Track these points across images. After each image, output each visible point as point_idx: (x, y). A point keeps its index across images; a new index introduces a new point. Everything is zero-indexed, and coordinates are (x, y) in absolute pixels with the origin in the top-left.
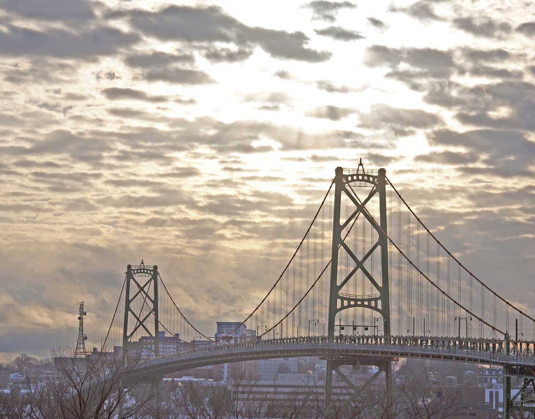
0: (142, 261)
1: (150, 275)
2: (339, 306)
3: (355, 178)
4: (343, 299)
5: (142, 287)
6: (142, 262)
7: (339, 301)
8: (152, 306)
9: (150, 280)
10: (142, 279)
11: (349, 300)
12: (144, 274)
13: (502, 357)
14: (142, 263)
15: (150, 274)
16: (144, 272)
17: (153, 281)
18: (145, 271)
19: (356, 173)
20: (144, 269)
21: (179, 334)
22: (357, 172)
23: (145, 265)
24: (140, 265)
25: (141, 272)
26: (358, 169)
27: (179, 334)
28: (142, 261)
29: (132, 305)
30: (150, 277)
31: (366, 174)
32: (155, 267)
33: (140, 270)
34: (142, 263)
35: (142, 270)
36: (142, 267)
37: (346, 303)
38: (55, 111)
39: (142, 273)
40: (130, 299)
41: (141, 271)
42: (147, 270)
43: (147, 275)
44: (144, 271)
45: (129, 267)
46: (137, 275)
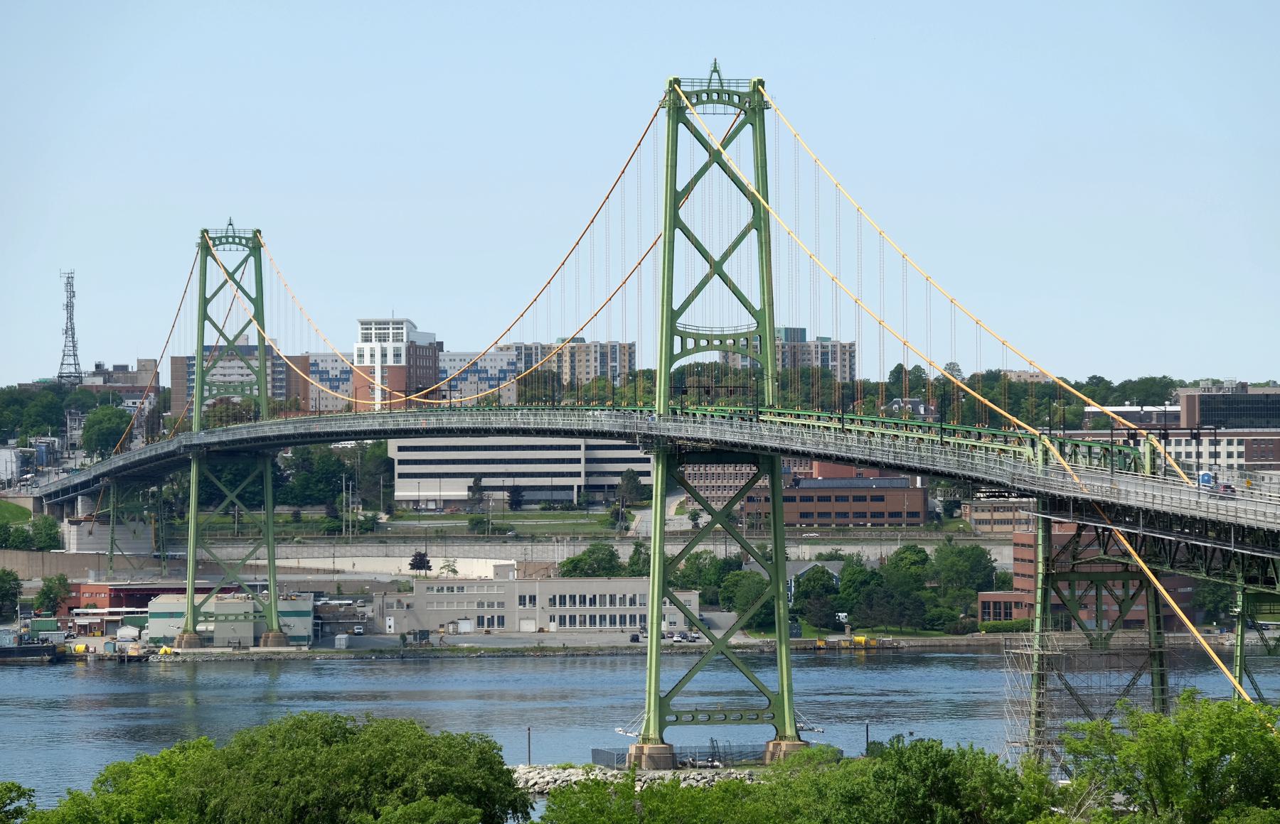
0: (715, 63)
1: (246, 249)
2: (677, 350)
3: (704, 97)
5: (231, 271)
6: (715, 67)
7: (677, 340)
8: (251, 309)
9: (245, 260)
10: (231, 256)
11: (697, 337)
12: (234, 247)
13: (943, 456)
14: (715, 70)
15: (246, 246)
16: (234, 243)
17: (252, 259)
18: (237, 240)
19: (706, 88)
20: (234, 237)
21: (594, 751)
22: (709, 86)
23: (235, 228)
24: (225, 227)
25: (228, 242)
26: (710, 80)
27: (594, 751)
28: (715, 63)
29: (211, 310)
30: (247, 251)
31: (726, 88)
33: (227, 237)
34: (715, 70)
35: (229, 239)
37: (690, 343)
38: (387, 579)
39: (231, 243)
40: (208, 296)
41: (227, 240)
42: (240, 238)
43: (240, 248)
44: (227, 240)
46: (221, 247)
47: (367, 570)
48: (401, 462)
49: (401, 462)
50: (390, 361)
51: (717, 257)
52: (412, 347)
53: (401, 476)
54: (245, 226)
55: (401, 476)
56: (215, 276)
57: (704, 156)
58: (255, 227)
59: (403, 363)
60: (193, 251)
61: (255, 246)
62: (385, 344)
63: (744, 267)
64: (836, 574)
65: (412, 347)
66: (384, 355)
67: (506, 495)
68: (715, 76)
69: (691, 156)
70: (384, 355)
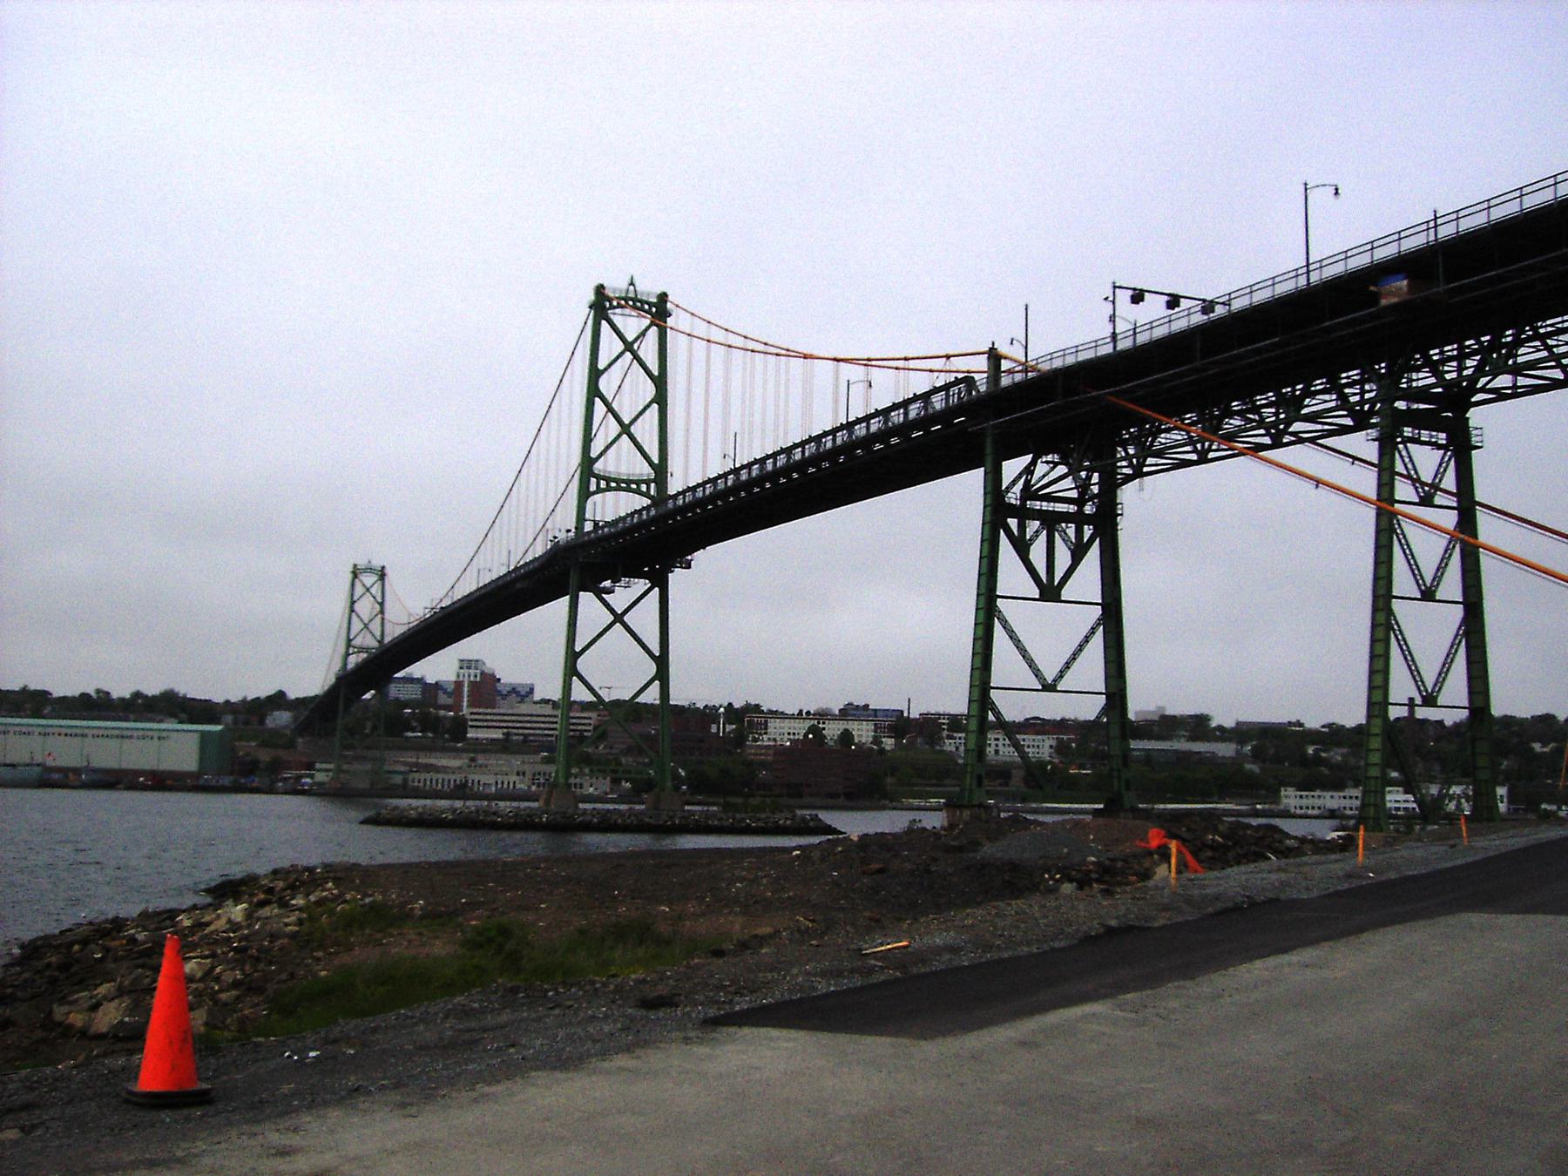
2: (593, 488)
4: (599, 478)
7: (593, 480)
10: (368, 580)
11: (608, 480)
14: (632, 284)
30: (376, 578)
32: (383, 568)
34: (632, 284)
35: (369, 570)
36: (631, 295)
45: (600, 290)
47: (970, 664)
48: (472, 720)
49: (472, 720)
50: (472, 679)
51: (627, 422)
52: (482, 673)
53: (471, 727)
54: (377, 563)
55: (471, 727)
56: (359, 590)
57: (620, 346)
58: (382, 565)
59: (478, 679)
60: (350, 576)
61: (382, 574)
62: (471, 671)
63: (647, 430)
64: (237, 743)
65: (482, 673)
66: (469, 676)
67: (521, 738)
68: (632, 288)
69: (610, 345)
70: (469, 676)
